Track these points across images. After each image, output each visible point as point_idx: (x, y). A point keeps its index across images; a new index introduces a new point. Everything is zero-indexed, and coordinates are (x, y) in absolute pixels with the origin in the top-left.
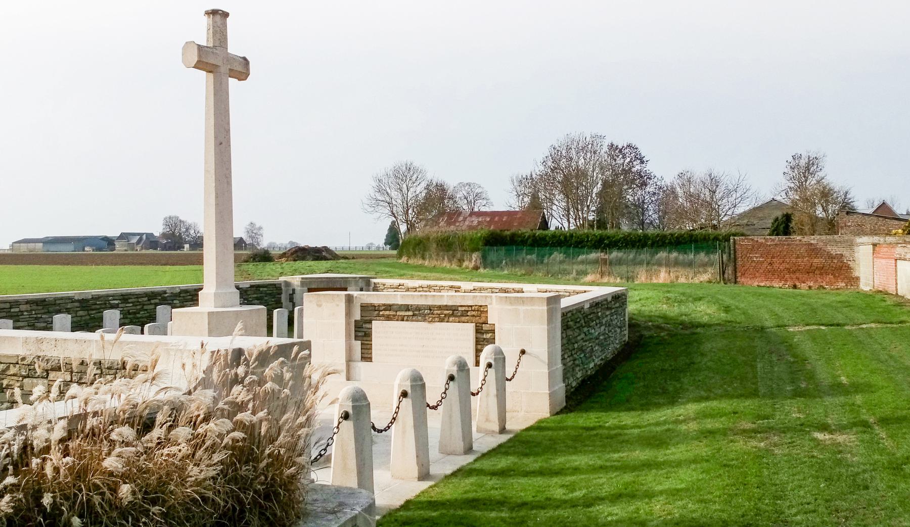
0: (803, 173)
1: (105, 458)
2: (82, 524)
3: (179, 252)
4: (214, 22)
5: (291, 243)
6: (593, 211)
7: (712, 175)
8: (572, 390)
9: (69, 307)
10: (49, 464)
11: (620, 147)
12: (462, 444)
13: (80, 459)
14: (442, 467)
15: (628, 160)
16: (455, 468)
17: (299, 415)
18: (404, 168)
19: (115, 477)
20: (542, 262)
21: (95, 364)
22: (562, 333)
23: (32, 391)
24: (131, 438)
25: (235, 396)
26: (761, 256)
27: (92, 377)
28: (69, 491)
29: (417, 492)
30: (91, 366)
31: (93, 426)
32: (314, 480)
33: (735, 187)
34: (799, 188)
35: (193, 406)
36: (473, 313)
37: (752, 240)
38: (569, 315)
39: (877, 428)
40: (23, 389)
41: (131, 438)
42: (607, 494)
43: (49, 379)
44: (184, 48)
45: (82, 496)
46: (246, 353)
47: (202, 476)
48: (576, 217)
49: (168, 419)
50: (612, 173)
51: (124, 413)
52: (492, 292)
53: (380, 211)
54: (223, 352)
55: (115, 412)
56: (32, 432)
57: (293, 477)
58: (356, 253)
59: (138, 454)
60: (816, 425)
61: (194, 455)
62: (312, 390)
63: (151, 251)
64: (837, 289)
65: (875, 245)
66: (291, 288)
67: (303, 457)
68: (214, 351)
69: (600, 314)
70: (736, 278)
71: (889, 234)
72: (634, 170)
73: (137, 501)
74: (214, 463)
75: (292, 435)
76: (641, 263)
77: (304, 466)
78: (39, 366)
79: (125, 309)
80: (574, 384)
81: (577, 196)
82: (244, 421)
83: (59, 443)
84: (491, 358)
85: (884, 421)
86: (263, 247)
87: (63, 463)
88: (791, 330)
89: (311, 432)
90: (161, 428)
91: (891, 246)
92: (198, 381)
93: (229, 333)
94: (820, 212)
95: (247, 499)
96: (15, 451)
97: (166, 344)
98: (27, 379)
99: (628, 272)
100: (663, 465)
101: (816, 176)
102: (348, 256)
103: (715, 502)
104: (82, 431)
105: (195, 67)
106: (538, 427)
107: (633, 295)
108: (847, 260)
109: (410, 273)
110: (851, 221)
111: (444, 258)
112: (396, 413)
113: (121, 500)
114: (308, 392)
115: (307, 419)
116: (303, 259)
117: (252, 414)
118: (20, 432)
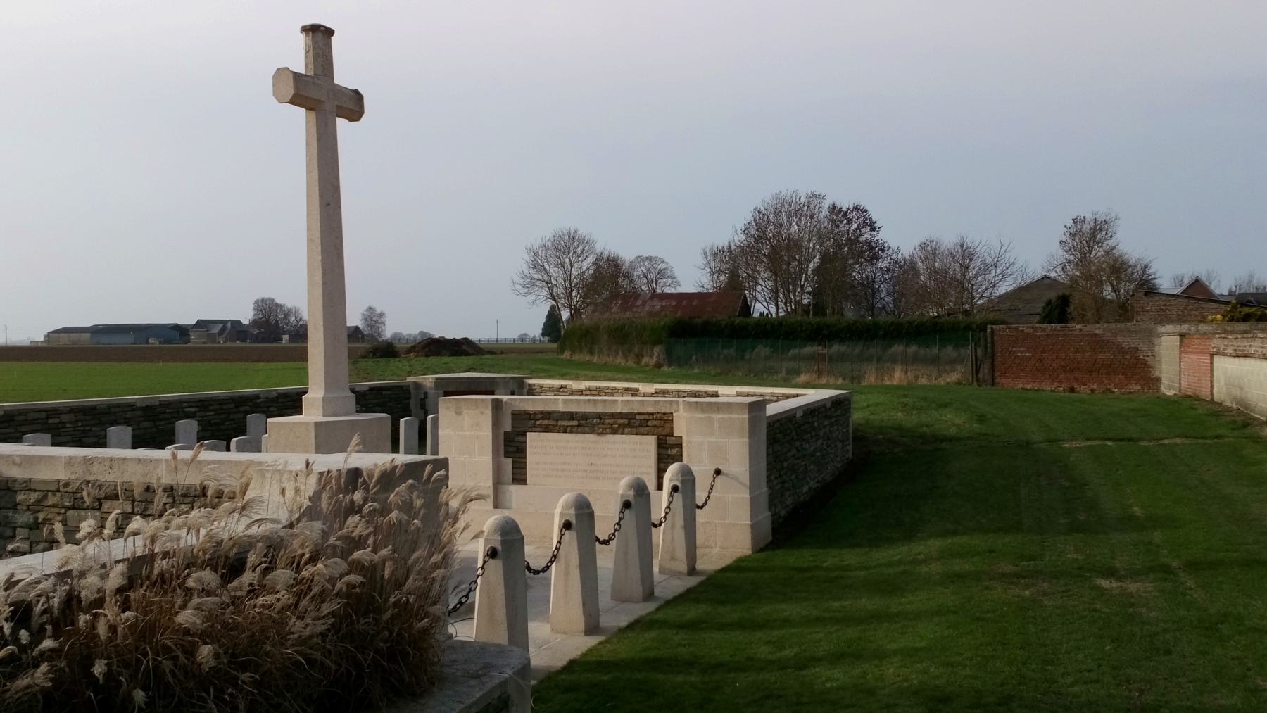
0: (1086, 242)
1: (178, 612)
2: (147, 698)
3: (275, 345)
4: (314, 42)
5: (422, 333)
6: (809, 293)
7: (965, 244)
8: (780, 520)
9: (128, 416)
10: (102, 621)
11: (844, 209)
12: (640, 589)
13: (145, 613)
14: (616, 617)
15: (855, 226)
16: (632, 618)
17: (433, 553)
18: (566, 238)
19: (192, 635)
20: (742, 359)
21: (165, 490)
22: (768, 448)
23: (78, 527)
24: (213, 585)
25: (350, 529)
26: (1028, 351)
27: (161, 507)
28: (129, 656)
29: (584, 649)
30: (160, 493)
31: (162, 570)
32: (452, 635)
33: (995, 261)
34: (1081, 261)
35: (296, 543)
36: (655, 422)
37: (1016, 329)
38: (777, 425)
39: (1182, 575)
40: (66, 525)
41: (213, 585)
42: (826, 653)
43: (102, 510)
44: (274, 77)
45: (148, 662)
46: (365, 474)
47: (307, 632)
48: (786, 300)
49: (263, 559)
50: (833, 243)
51: (205, 553)
52: (679, 396)
53: (536, 293)
54: (334, 473)
55: (192, 552)
56: (79, 580)
57: (426, 631)
58: (513, 346)
59: (224, 606)
60: (1099, 569)
61: (297, 605)
62: (450, 520)
63: (238, 344)
64: (1130, 393)
65: (1182, 336)
66: (423, 391)
67: (438, 606)
68: (324, 472)
69: (816, 424)
70: (993, 378)
71: (1203, 321)
72: (863, 239)
73: (222, 666)
74: (323, 615)
75: (425, 579)
76: (869, 359)
77: (439, 617)
78: (89, 495)
79: (205, 418)
80: (783, 513)
81: (789, 274)
82: (362, 561)
83: (116, 594)
84: (678, 480)
85: (1193, 566)
86: (386, 338)
87: (121, 620)
88: (1067, 445)
89: (448, 574)
90: (253, 571)
91: (1206, 337)
92: (302, 510)
93: (342, 449)
94: (1108, 293)
95: (366, 660)
96: (56, 605)
97: (260, 463)
98: (72, 512)
99: (852, 370)
100: (897, 617)
101: (1104, 245)
102: (494, 350)
103: (965, 666)
104: (148, 578)
105: (291, 102)
106: (738, 567)
107: (859, 400)
108: (1144, 356)
109: (574, 372)
110: (1149, 304)
111: (617, 354)
112: (556, 549)
113: (200, 665)
114: (445, 523)
115: (444, 558)
116: (438, 354)
117: (372, 551)
118: (62, 580)
